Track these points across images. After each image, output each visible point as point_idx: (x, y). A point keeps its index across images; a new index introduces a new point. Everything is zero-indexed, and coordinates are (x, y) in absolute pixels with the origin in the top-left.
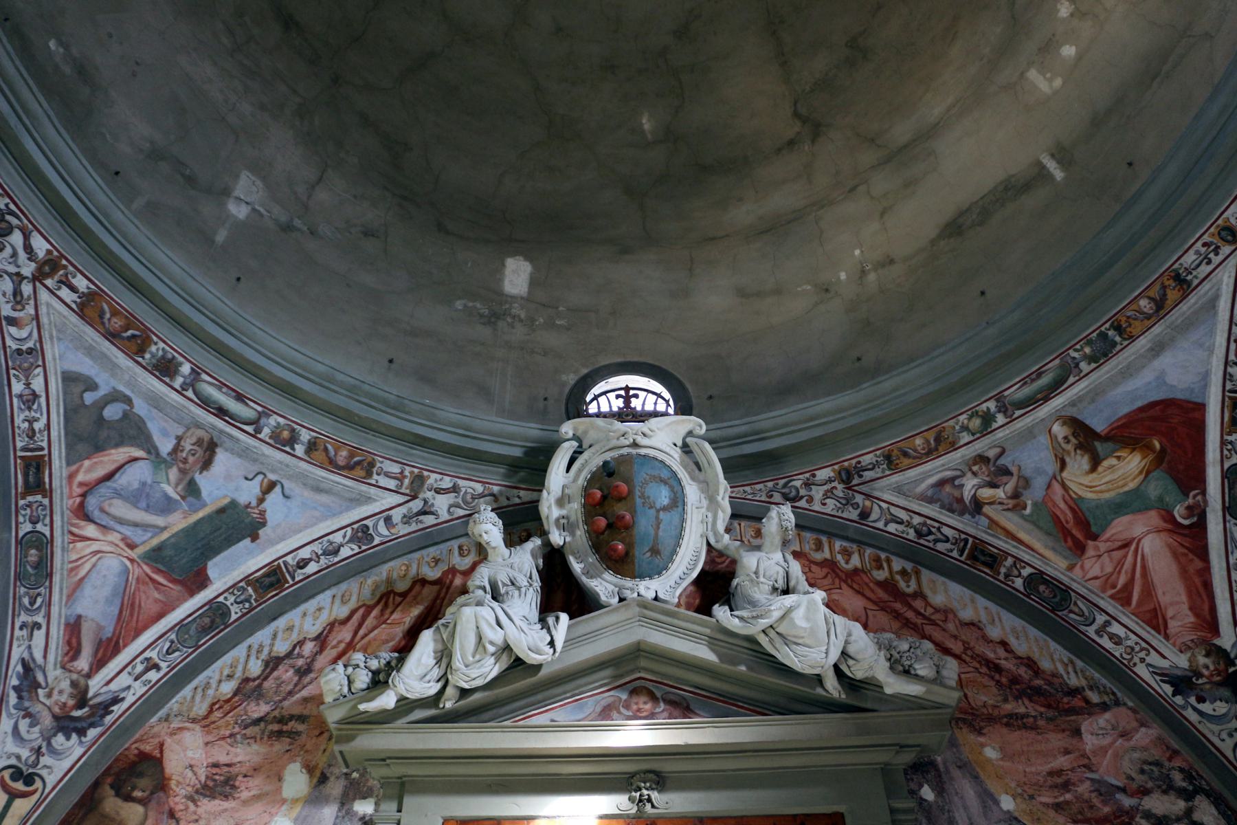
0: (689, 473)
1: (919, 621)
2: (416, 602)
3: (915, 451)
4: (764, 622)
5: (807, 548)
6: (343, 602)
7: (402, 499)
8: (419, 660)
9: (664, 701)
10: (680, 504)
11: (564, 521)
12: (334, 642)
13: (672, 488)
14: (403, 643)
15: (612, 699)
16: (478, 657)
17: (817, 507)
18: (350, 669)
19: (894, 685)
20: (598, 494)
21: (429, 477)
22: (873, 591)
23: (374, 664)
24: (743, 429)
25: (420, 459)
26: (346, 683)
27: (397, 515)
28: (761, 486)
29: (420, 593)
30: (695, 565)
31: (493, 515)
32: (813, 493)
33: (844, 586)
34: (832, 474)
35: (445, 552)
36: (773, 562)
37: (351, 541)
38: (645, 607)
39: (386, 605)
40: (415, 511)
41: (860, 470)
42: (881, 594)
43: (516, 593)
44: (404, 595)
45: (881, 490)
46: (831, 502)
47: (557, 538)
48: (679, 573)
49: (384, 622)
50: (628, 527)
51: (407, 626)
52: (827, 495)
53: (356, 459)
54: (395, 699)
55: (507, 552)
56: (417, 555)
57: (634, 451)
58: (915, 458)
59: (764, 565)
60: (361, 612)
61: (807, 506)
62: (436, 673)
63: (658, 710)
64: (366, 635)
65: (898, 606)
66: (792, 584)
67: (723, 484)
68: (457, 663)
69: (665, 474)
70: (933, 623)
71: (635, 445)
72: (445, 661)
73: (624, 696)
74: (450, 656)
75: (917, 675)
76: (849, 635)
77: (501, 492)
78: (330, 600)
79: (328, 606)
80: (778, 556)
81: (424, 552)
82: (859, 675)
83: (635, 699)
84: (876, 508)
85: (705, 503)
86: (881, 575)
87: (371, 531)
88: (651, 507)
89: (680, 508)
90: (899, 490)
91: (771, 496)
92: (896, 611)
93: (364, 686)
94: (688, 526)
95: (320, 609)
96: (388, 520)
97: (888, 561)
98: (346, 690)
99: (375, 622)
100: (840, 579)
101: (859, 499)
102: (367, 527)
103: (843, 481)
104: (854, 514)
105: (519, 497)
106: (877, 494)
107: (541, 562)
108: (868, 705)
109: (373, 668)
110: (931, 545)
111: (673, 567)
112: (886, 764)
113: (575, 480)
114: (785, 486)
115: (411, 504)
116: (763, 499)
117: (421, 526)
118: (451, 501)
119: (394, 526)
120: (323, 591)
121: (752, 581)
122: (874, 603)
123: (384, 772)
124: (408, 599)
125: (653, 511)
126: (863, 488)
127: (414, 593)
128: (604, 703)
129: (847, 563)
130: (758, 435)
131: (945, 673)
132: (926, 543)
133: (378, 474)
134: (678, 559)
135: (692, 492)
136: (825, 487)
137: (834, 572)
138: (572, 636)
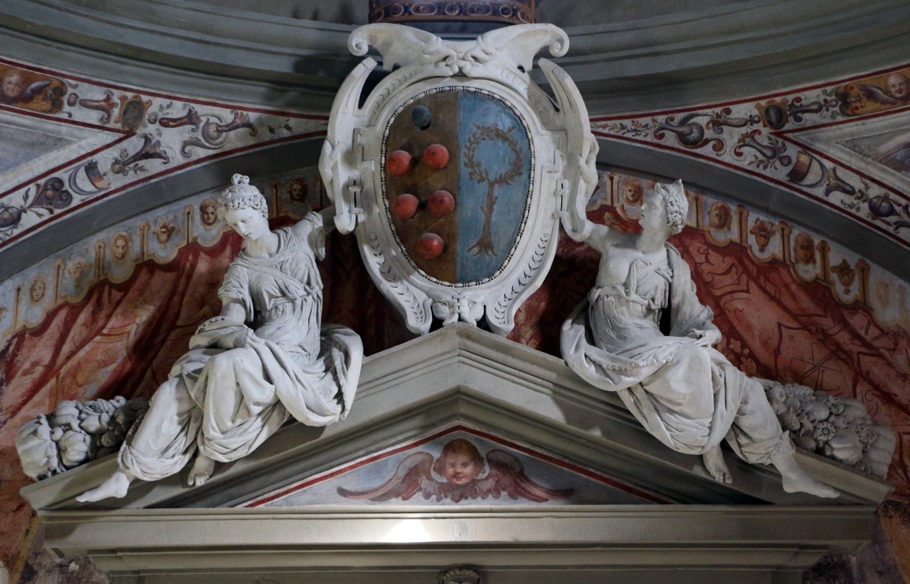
0: (540, 114)
1: (855, 348)
2: (143, 299)
3: (887, 92)
4: (630, 381)
5: (706, 223)
7: (109, 137)
8: (158, 428)
9: (490, 461)
10: (524, 170)
11: (357, 189)
12: (27, 365)
13: (513, 144)
14: (128, 366)
15: (420, 458)
17: (728, 157)
18: (59, 433)
19: (795, 482)
20: (405, 157)
21: (150, 103)
22: (794, 297)
23: (93, 423)
24: (628, 37)
25: (134, 79)
26: (55, 452)
27: (105, 161)
28: (643, 121)
29: (147, 284)
30: (542, 262)
32: (724, 136)
33: (753, 287)
34: (755, 112)
35: (180, 217)
36: (651, 269)
37: (37, 202)
38: (468, 337)
39: (99, 305)
40: (132, 153)
41: (798, 110)
42: (806, 302)
43: (289, 306)
44: (125, 287)
45: (828, 142)
46: (749, 152)
47: (345, 222)
48: (518, 274)
49: (99, 332)
50: (447, 214)
51: (132, 338)
52: (743, 143)
53: (34, 85)
55: (271, 239)
57: (459, 85)
58: (884, 102)
59: (642, 272)
60: (63, 314)
61: (713, 155)
62: (183, 442)
63: (481, 476)
65: (827, 322)
66: (675, 301)
67: (591, 171)
68: (212, 430)
69: (505, 123)
70: (874, 352)
71: (461, 75)
72: (193, 426)
73: (437, 454)
74: (201, 417)
75: (833, 458)
76: (745, 402)
77: (260, 121)
78: (12, 296)
79: (11, 306)
80: (659, 257)
82: (753, 459)
83: (450, 459)
84: (815, 166)
85: (561, 164)
86: (809, 272)
87: (66, 187)
88: (481, 180)
89: (525, 176)
90: (853, 145)
91: (662, 136)
92: (823, 331)
93: (81, 457)
94: (534, 203)
96: (91, 169)
97: (824, 249)
98: (55, 463)
99: (85, 333)
100: (749, 275)
101: (792, 151)
102: (61, 182)
103: (770, 123)
104: (781, 173)
105: (288, 128)
106: (819, 146)
107: (322, 252)
108: (762, 496)
109: (92, 429)
110: (891, 229)
111: (510, 265)
112: (779, 567)
113: (371, 124)
114: (683, 122)
115: (125, 144)
116: (649, 139)
117: (142, 175)
118: (187, 137)
119: (101, 177)
121: (619, 297)
122: (794, 316)
123: (116, 566)
124: (131, 295)
125: (484, 187)
126: (802, 137)
127: (138, 284)
128: (409, 464)
129: (762, 250)
130: (650, 48)
131: (874, 455)
132: (884, 226)
133: (71, 104)
134: (517, 253)
135: (543, 145)
136: (744, 130)
137: (741, 262)
138: (363, 382)
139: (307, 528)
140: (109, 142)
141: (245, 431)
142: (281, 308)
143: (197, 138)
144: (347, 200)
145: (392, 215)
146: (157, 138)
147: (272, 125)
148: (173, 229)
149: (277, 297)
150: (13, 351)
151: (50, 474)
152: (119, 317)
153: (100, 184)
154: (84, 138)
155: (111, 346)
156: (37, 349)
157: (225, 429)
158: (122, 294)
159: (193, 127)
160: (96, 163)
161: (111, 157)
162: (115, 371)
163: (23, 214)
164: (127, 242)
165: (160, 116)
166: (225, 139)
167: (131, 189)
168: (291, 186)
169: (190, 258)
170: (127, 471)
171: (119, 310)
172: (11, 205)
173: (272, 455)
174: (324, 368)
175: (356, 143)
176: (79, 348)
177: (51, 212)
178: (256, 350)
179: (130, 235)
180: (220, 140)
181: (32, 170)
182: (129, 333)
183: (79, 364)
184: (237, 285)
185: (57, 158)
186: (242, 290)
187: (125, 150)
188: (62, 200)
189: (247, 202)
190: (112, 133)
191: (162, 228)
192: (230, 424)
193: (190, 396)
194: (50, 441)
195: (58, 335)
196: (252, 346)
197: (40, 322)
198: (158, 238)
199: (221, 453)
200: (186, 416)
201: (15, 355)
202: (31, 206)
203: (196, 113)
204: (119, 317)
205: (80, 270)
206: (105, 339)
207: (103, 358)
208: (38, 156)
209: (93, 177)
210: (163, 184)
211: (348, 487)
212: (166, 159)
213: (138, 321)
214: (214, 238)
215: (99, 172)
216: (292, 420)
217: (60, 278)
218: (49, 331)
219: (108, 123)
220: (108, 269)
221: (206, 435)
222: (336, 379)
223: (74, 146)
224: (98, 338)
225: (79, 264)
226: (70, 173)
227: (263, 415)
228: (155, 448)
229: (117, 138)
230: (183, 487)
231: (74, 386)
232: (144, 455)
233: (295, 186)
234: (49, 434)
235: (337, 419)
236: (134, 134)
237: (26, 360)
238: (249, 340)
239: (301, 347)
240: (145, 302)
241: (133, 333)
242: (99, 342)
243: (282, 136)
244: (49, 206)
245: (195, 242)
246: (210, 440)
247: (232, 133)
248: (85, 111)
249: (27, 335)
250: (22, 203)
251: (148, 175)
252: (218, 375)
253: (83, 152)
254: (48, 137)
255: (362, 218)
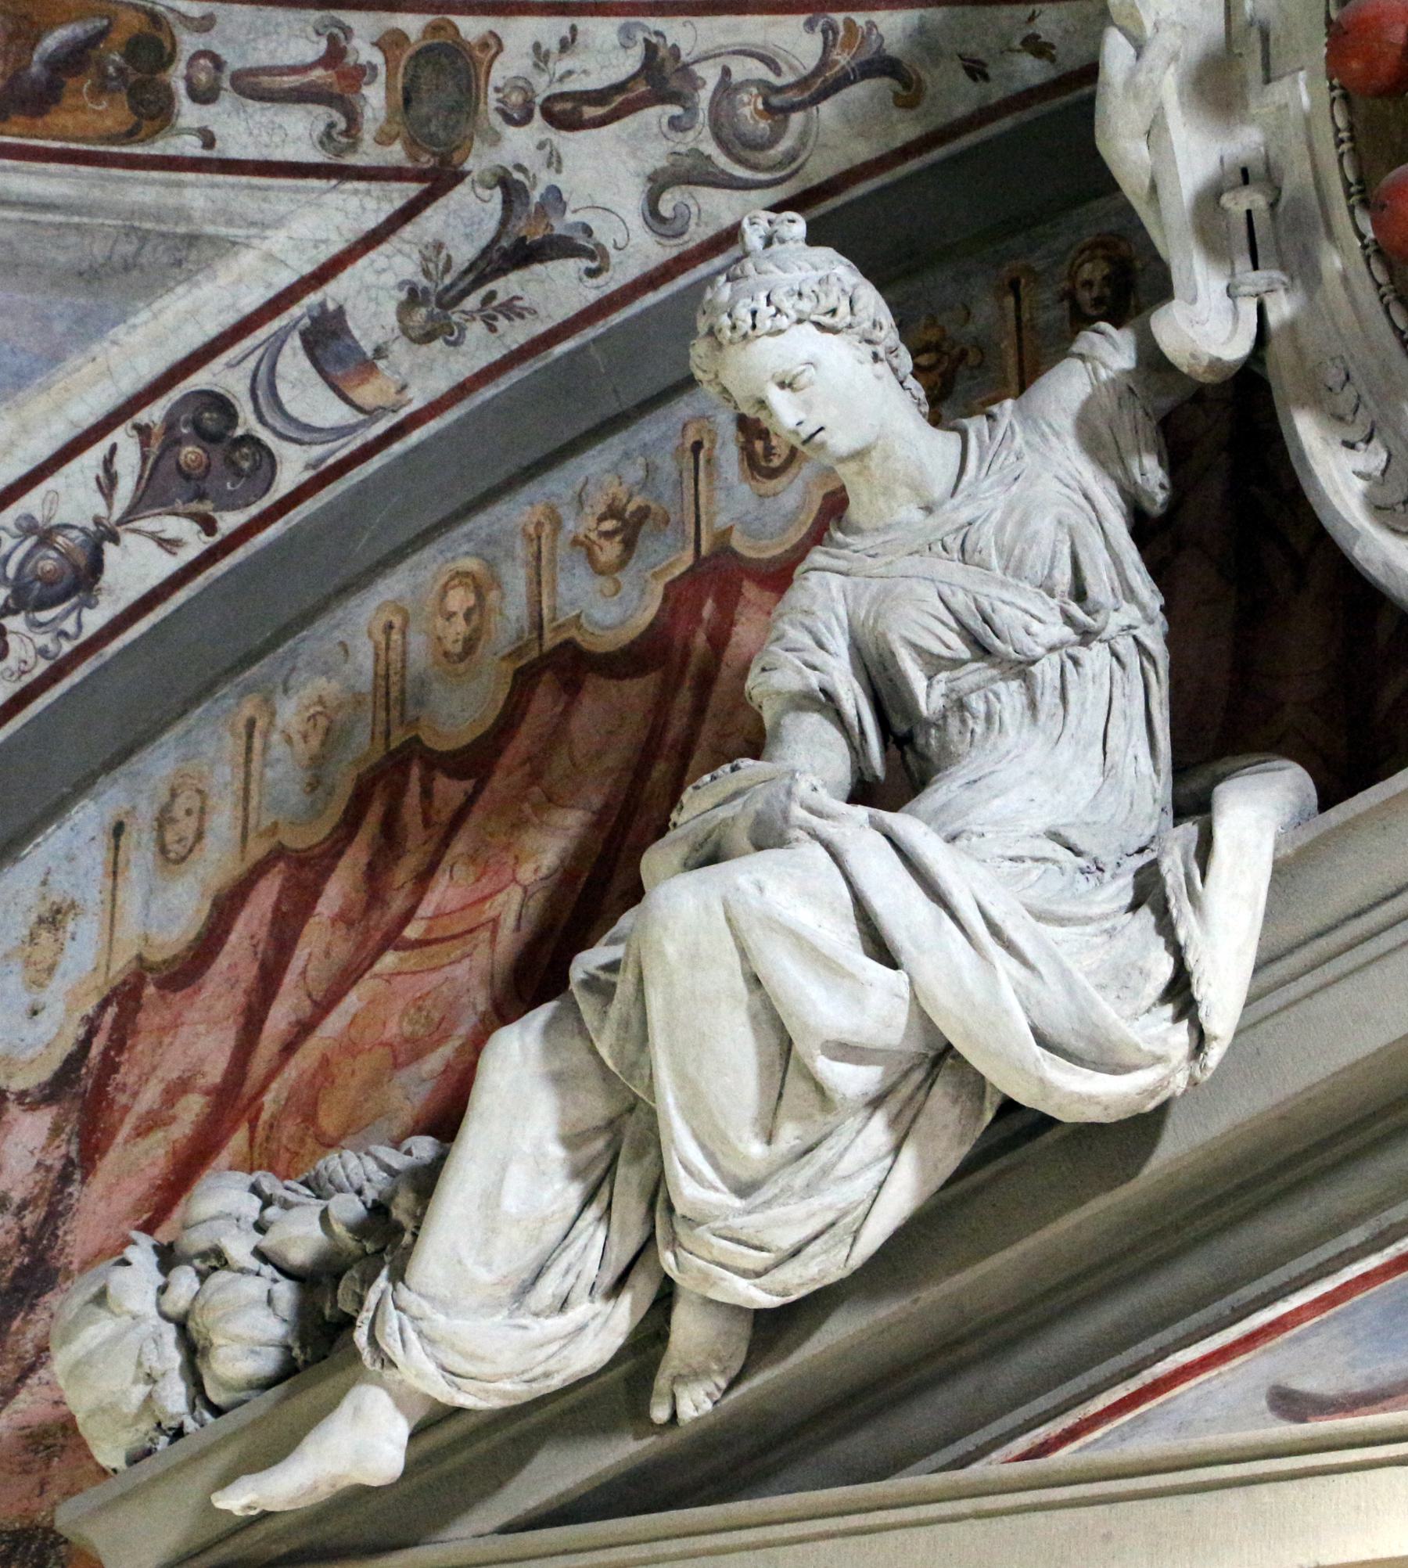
6: (171, 858)
7: (361, 207)
8: (491, 1199)
11: (1254, 199)
12: (150, 1097)
16: (789, 1135)
18: (185, 1281)
21: (493, 44)
23: (301, 1235)
26: (175, 1358)
27: (369, 298)
29: (557, 735)
31: (837, 270)
35: (667, 465)
40: (464, 253)
43: (1011, 694)
44: (475, 761)
49: (392, 940)
53: (52, 41)
54: (401, 1429)
55: (932, 450)
56: (517, 512)
62: (592, 1250)
64: (304, 1029)
68: (695, 1188)
72: (629, 1179)
78: (96, 857)
79: (92, 894)
81: (558, 484)
87: (247, 422)
93: (266, 1363)
95: (54, 919)
96: (326, 340)
98: (175, 1397)
99: (342, 950)
102: (221, 404)
105: (1037, 47)
107: (1151, 474)
109: (299, 1255)
115: (433, 221)
117: (517, 334)
118: (656, 155)
119: (367, 367)
120: (56, 811)
124: (499, 782)
127: (522, 742)
133: (203, 96)
138: (1290, 932)
139: (1107, 1537)
140: (371, 222)
141: (825, 1171)
142: (977, 703)
143: (696, 153)
144: (1215, 247)
145: (1389, 268)
146: (546, 178)
147: (972, 48)
148: (643, 513)
149: (956, 663)
150: (105, 1054)
151: (163, 1440)
152: (460, 871)
153: (366, 394)
154: (279, 222)
155: (435, 978)
156: (185, 1032)
157: (745, 1175)
158: (468, 785)
159: (676, 110)
160: (340, 311)
161: (390, 279)
162: (448, 1067)
163: (109, 548)
164: (480, 596)
165: (543, 88)
166: (804, 134)
167: (487, 393)
168: (1072, 276)
169: (708, 609)
170: (388, 1374)
171: (460, 846)
172: (55, 522)
173: (960, 1268)
174: (1127, 898)
175: (1238, 21)
176: (324, 1007)
177: (208, 525)
178: (828, 846)
179: (491, 564)
180: (786, 144)
181: (109, 372)
182: (495, 922)
183: (325, 1062)
184: (805, 648)
185: (193, 313)
186: (819, 657)
187: (439, 246)
188: (239, 473)
189: (787, 305)
190: (375, 187)
191: (602, 519)
192: (756, 1149)
193: (601, 1062)
194: (154, 1319)
195: (254, 970)
196: (814, 836)
197: (192, 935)
198: (591, 557)
199: (745, 1274)
200: (599, 1144)
201: (109, 1066)
202: (132, 513)
203: (675, 51)
204: (460, 871)
205: (322, 722)
206: (412, 959)
207: (407, 1029)
208: (122, 318)
209: (337, 373)
210: (592, 349)
211: (1310, 1384)
212: (597, 259)
213: (526, 873)
214: (791, 519)
215: (356, 348)
216: (1009, 1107)
217: (255, 766)
218: (222, 962)
219: (353, 147)
220: (420, 703)
221: (680, 1210)
222: (1166, 927)
223: (248, 259)
224: (389, 960)
225: (321, 701)
226: (251, 363)
227: (893, 1104)
228: (484, 1276)
229: (398, 203)
230: (638, 1437)
231: (310, 1142)
232: (445, 1305)
233: (1086, 271)
234: (152, 1296)
235: (1180, 1082)
236: (459, 177)
237: (144, 1079)
238: (798, 813)
239: (1055, 836)
240: (552, 800)
241: (509, 921)
242: (391, 977)
243: (1018, 86)
244: (195, 507)
245: (724, 549)
246: (691, 1222)
247: (826, 108)
248: (261, 114)
249: (150, 990)
250: (99, 506)
251: (540, 328)
252: (670, 949)
253: (285, 279)
254: (144, 237)
255: (1281, 309)
